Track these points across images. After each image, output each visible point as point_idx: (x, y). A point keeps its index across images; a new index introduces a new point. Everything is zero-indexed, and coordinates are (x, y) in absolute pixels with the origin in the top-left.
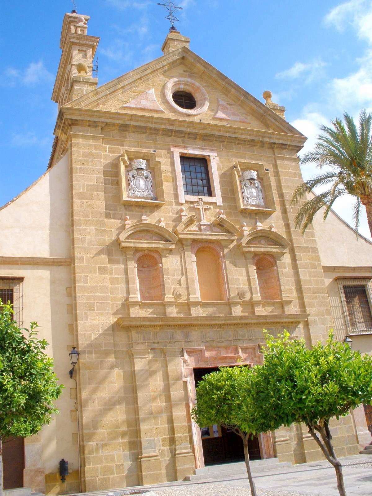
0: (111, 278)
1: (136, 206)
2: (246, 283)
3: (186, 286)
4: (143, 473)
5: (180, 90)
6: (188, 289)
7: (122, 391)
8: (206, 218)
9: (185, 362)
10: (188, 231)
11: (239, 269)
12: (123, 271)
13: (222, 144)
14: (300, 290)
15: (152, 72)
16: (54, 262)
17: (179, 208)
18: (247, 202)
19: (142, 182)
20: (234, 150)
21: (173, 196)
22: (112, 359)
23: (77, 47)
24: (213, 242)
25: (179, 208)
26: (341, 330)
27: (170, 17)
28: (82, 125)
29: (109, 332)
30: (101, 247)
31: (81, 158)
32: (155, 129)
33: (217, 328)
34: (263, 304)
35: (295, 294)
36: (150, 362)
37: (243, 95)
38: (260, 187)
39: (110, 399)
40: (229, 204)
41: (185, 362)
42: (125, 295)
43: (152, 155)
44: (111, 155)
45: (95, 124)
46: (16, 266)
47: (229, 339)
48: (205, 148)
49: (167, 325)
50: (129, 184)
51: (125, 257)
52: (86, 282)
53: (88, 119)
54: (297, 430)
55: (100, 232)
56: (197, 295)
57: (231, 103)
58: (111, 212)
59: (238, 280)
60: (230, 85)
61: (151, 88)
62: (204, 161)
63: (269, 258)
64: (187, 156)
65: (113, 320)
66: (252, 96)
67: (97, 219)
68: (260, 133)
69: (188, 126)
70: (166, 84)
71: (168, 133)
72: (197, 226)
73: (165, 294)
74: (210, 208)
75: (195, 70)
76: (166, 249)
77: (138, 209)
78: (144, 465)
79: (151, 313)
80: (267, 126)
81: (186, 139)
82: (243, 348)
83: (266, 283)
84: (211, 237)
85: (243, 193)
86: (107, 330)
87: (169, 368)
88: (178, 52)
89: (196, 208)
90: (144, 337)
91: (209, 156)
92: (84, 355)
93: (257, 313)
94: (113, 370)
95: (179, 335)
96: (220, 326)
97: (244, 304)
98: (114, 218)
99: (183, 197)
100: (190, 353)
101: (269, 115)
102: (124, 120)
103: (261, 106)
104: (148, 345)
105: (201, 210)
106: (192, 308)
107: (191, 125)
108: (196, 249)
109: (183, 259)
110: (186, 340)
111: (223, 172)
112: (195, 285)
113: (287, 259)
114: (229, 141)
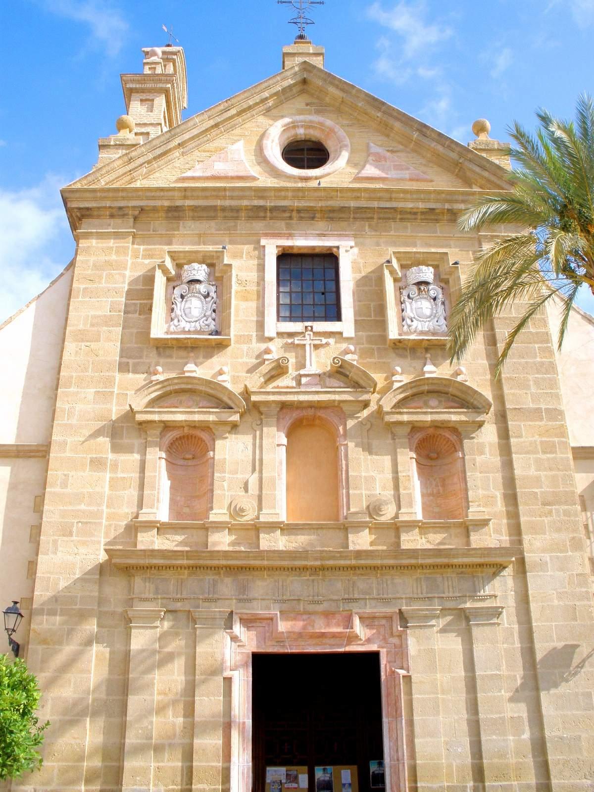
0: (112, 479)
1: (180, 348)
3: (257, 493)
5: (299, 138)
6: (260, 498)
7: (104, 688)
8: (318, 362)
9: (234, 639)
11: (377, 457)
12: (138, 464)
13: (367, 223)
14: (512, 498)
15: (239, 114)
16: (19, 451)
17: (263, 346)
18: (409, 326)
20: (392, 233)
21: (253, 326)
22: (92, 626)
23: (138, 95)
24: (326, 408)
25: (263, 346)
27: (298, 20)
28: (98, 217)
29: (92, 577)
30: (101, 424)
31: (89, 272)
32: (232, 209)
33: (310, 576)
35: (500, 506)
36: (163, 637)
37: (418, 130)
38: (440, 296)
39: (75, 704)
41: (234, 639)
42: (135, 510)
43: (218, 254)
44: (147, 261)
45: (121, 213)
47: (335, 597)
48: (331, 233)
49: (200, 565)
50: (173, 310)
51: (145, 441)
52: (64, 485)
55: (104, 396)
56: (279, 509)
57: (395, 149)
59: (370, 480)
60: (391, 115)
62: (330, 258)
63: (447, 434)
64: (295, 251)
65: (103, 557)
66: (433, 130)
67: (102, 374)
68: (443, 195)
69: (293, 197)
71: (257, 213)
73: (212, 509)
75: (327, 99)
76: (224, 423)
79: (181, 543)
80: (468, 182)
81: (294, 222)
82: (366, 615)
83: (443, 486)
84: (316, 398)
85: (403, 310)
86: (89, 572)
87: (198, 650)
88: (293, 71)
90: (157, 589)
91: (338, 247)
92: (40, 617)
93: (404, 546)
94: (89, 648)
95: (227, 586)
96: (315, 570)
97: (377, 528)
98: (135, 372)
99: (272, 325)
100: (248, 622)
102: (171, 199)
103: (453, 146)
104: (162, 604)
105: (308, 348)
106: (262, 536)
109: (258, 441)
110: (241, 596)
111: (363, 274)
112: (275, 489)
113: (489, 434)
114: (382, 215)
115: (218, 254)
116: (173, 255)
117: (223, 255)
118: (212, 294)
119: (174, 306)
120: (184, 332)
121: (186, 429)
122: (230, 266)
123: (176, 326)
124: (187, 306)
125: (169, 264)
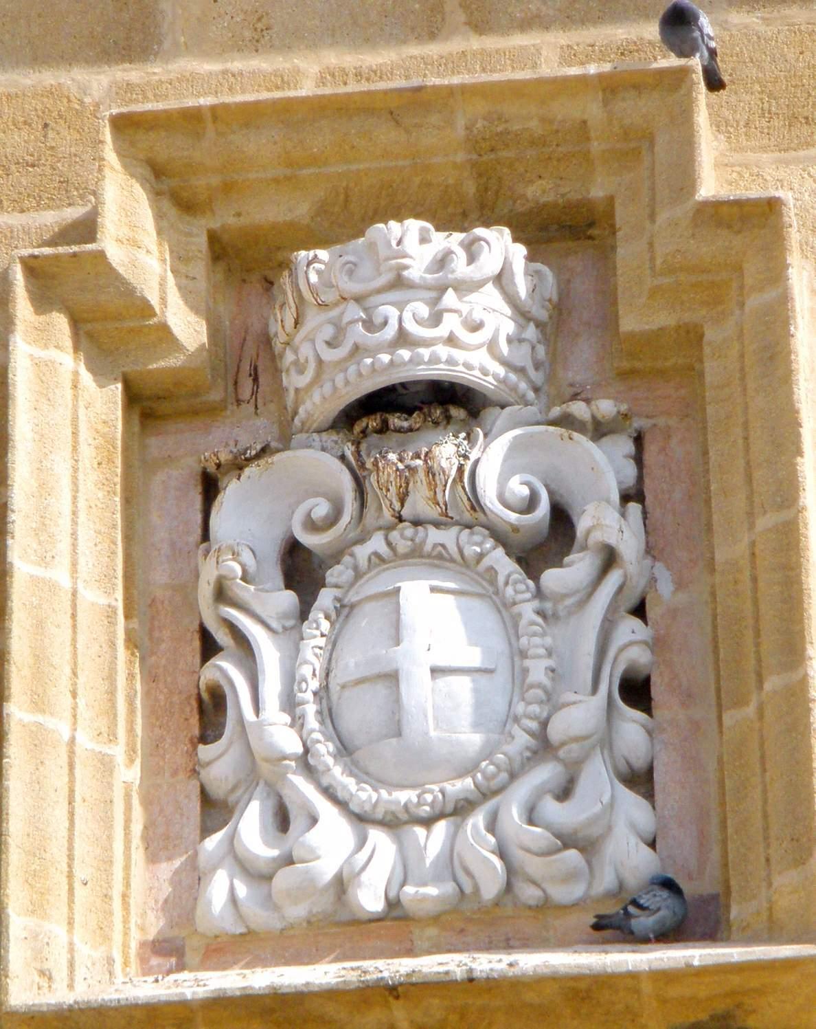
19: (438, 640)
43: (634, 109)
50: (211, 710)
115: (634, 109)
116: (170, 156)
117: (684, 118)
118: (603, 520)
119: (227, 668)
120: (338, 923)
121: (442, 975)
122: (757, 219)
123: (261, 876)
124: (351, 662)
125: (136, 241)
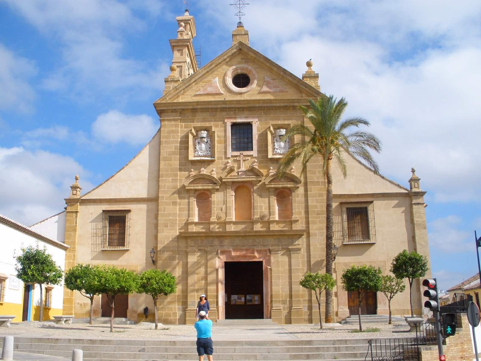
2: (268, 208)
4: (187, 318)
5: (239, 73)
10: (230, 176)
14: (307, 212)
25: (227, 161)
26: (340, 239)
28: (167, 112)
34: (260, 223)
40: (262, 155)
44: (186, 129)
46: (128, 203)
47: (249, 245)
50: (196, 148)
52: (164, 211)
53: (170, 108)
54: (290, 304)
58: (183, 167)
61: (216, 77)
62: (249, 125)
63: (287, 190)
70: (226, 72)
71: (223, 110)
72: (236, 173)
74: (248, 159)
77: (200, 164)
78: (187, 314)
83: (286, 207)
89: (238, 160)
91: (252, 122)
93: (271, 229)
95: (216, 242)
96: (243, 236)
98: (185, 171)
99: (230, 153)
101: (302, 84)
106: (227, 225)
107: (239, 102)
108: (234, 187)
111: (261, 132)
113: (301, 190)
116: (195, 128)
125: (193, 131)
